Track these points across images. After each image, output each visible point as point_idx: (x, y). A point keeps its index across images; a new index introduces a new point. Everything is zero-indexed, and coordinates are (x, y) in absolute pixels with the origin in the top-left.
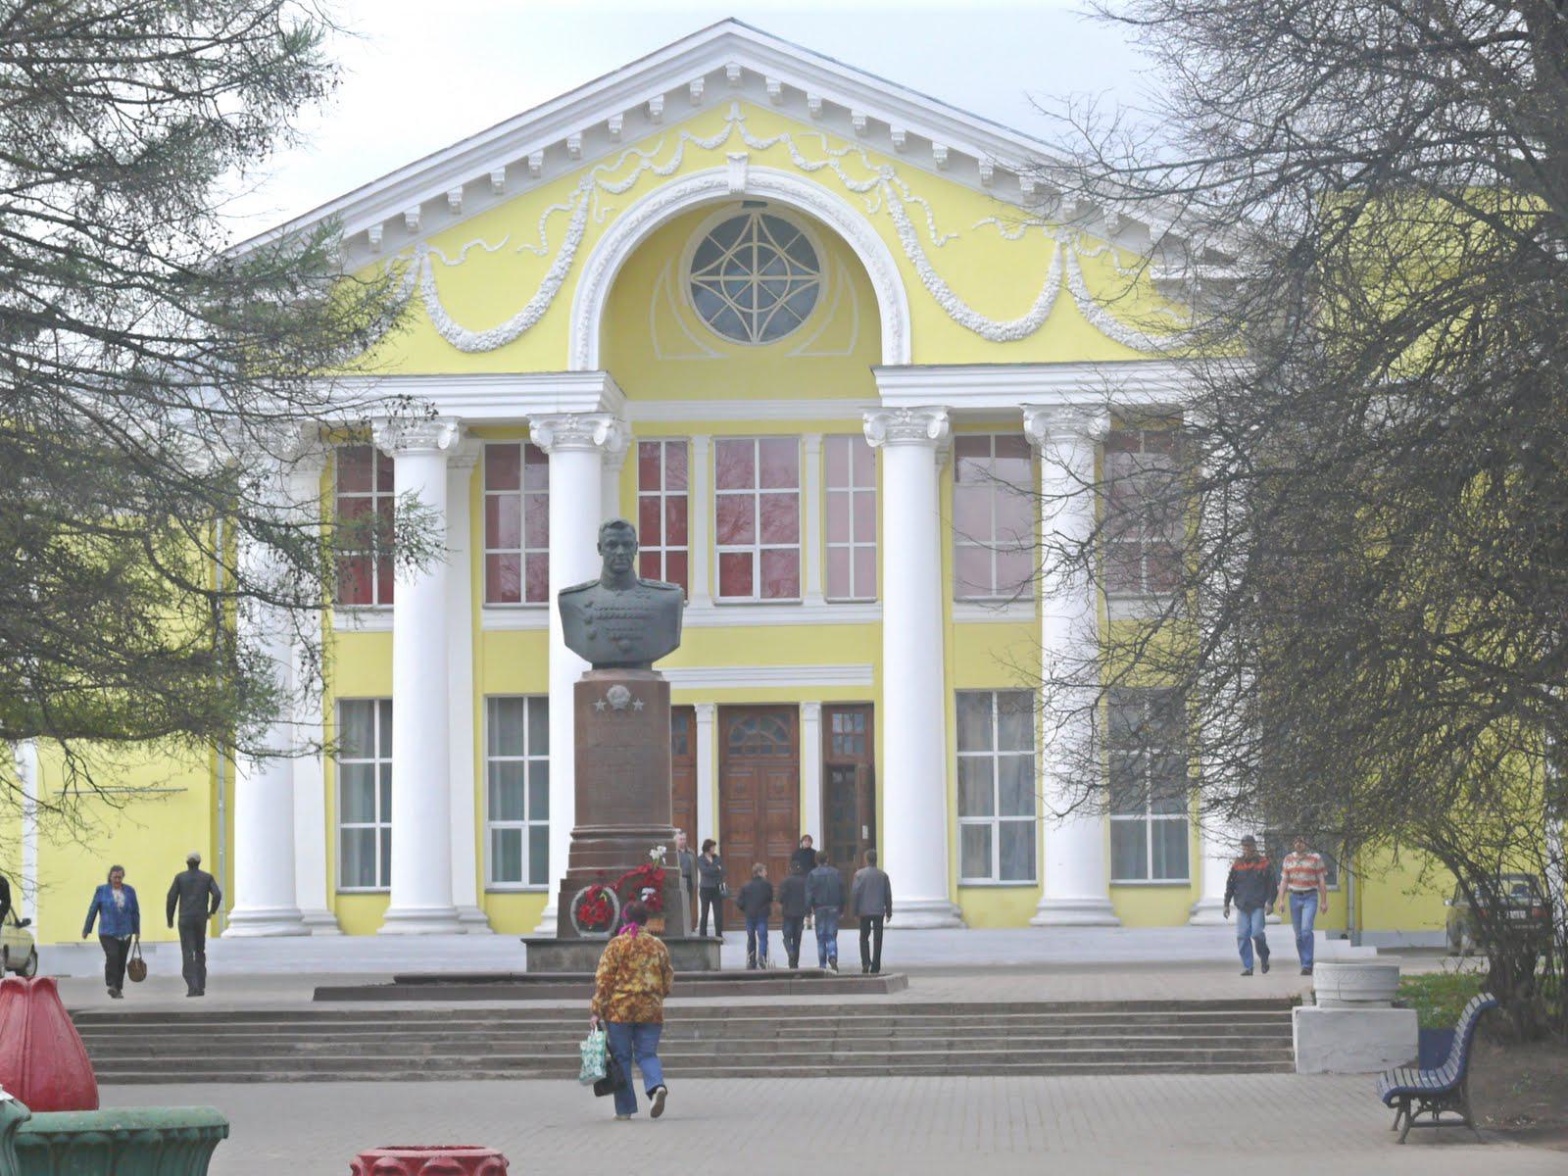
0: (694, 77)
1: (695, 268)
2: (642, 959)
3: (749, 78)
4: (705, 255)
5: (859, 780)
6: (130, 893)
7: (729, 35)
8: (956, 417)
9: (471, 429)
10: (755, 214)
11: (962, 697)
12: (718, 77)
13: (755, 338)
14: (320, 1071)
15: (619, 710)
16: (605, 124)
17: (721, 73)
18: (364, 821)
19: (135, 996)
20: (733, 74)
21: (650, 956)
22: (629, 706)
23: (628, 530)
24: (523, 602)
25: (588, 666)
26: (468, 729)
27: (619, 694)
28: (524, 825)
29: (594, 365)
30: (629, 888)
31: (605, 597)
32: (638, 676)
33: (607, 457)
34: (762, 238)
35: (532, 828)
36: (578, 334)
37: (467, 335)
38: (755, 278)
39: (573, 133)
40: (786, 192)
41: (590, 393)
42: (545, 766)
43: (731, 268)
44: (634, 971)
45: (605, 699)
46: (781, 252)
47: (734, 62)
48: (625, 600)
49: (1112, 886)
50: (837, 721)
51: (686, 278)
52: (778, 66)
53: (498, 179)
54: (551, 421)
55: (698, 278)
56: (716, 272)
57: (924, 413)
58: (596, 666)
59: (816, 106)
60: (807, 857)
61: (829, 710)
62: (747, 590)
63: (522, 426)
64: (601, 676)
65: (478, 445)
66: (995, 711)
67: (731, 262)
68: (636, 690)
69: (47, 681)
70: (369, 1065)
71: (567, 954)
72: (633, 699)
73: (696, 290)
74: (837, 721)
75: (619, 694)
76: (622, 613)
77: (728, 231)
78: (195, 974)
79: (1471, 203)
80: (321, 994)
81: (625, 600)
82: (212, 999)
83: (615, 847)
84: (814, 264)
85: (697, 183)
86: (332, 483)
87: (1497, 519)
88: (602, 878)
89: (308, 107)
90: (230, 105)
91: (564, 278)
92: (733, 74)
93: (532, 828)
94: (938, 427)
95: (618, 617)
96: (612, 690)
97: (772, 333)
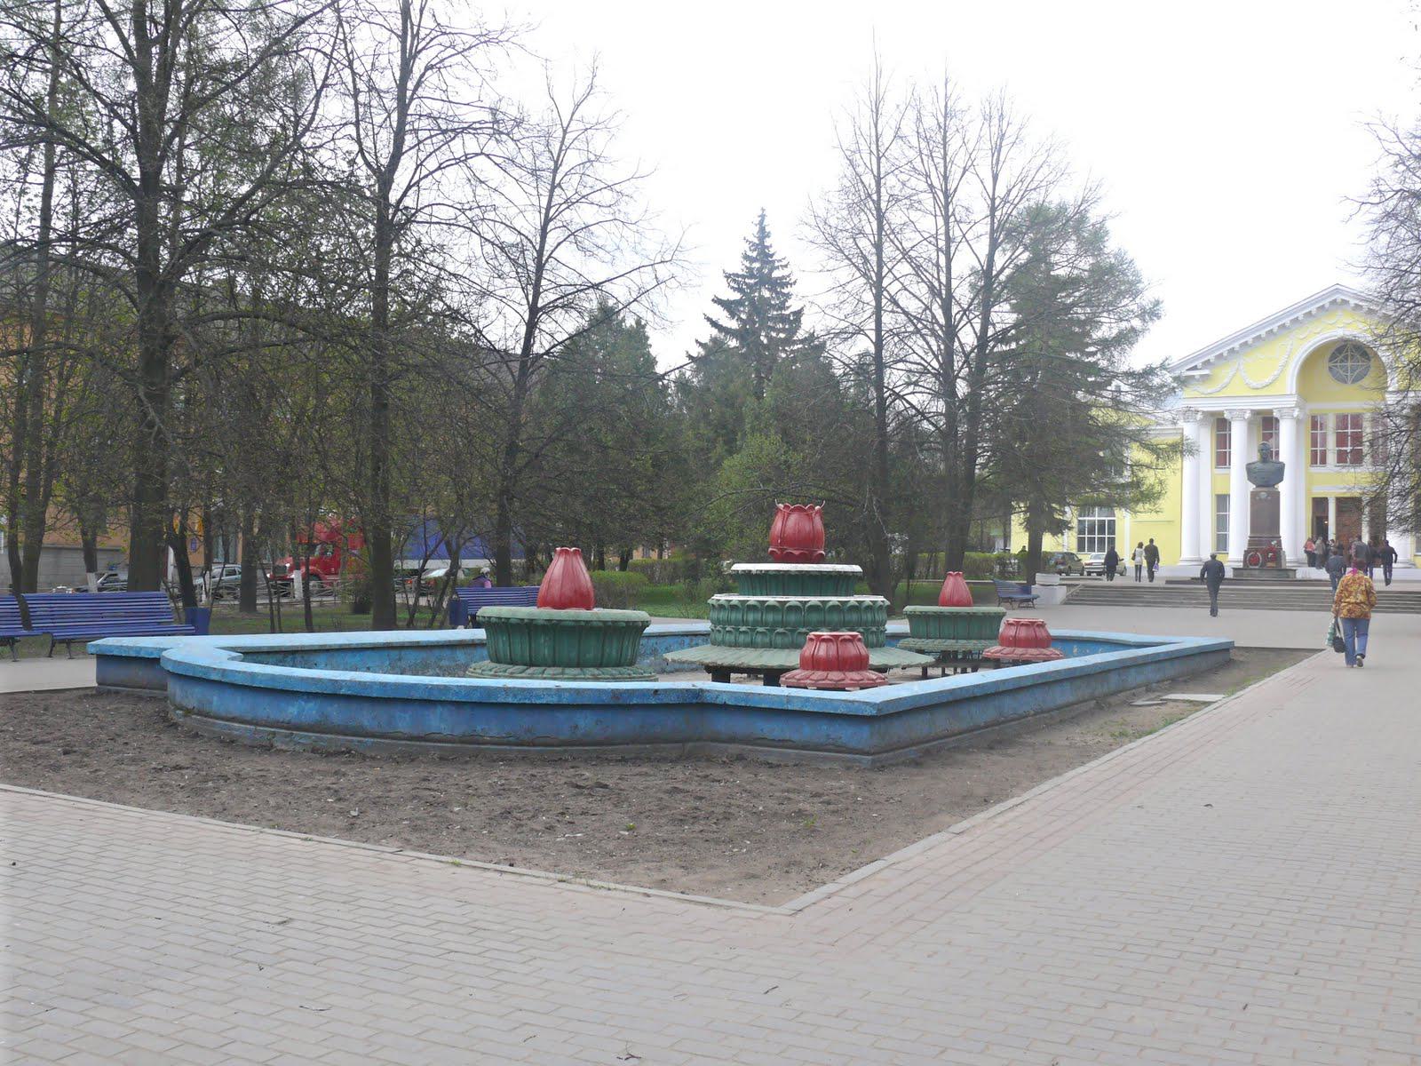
0: (1326, 302)
1: (1330, 361)
2: (1355, 587)
3: (1345, 302)
9: (1256, 413)
12: (1334, 302)
14: (1148, 604)
17: (1335, 300)
19: (1118, 581)
20: (1339, 301)
21: (1360, 585)
27: (1263, 495)
29: (1294, 392)
30: (1265, 553)
31: (1260, 465)
32: (1270, 489)
33: (1298, 421)
36: (1290, 383)
37: (1254, 384)
38: (1349, 364)
43: (1342, 361)
44: (1351, 592)
47: (1339, 297)
48: (1268, 467)
51: (1327, 364)
52: (1312, 305)
54: (1280, 410)
55: (1331, 364)
57: (1243, 411)
58: (1258, 486)
63: (1271, 411)
64: (1259, 489)
65: (1259, 418)
68: (1269, 494)
70: (1164, 603)
71: (1245, 572)
73: (1330, 368)
75: (1263, 495)
78: (1151, 576)
80: (1168, 582)
81: (1268, 467)
85: (1327, 335)
88: (1257, 550)
89: (1157, 322)
90: (1136, 323)
91: (1284, 366)
92: (1339, 301)
94: (1248, 415)
97: (1354, 381)
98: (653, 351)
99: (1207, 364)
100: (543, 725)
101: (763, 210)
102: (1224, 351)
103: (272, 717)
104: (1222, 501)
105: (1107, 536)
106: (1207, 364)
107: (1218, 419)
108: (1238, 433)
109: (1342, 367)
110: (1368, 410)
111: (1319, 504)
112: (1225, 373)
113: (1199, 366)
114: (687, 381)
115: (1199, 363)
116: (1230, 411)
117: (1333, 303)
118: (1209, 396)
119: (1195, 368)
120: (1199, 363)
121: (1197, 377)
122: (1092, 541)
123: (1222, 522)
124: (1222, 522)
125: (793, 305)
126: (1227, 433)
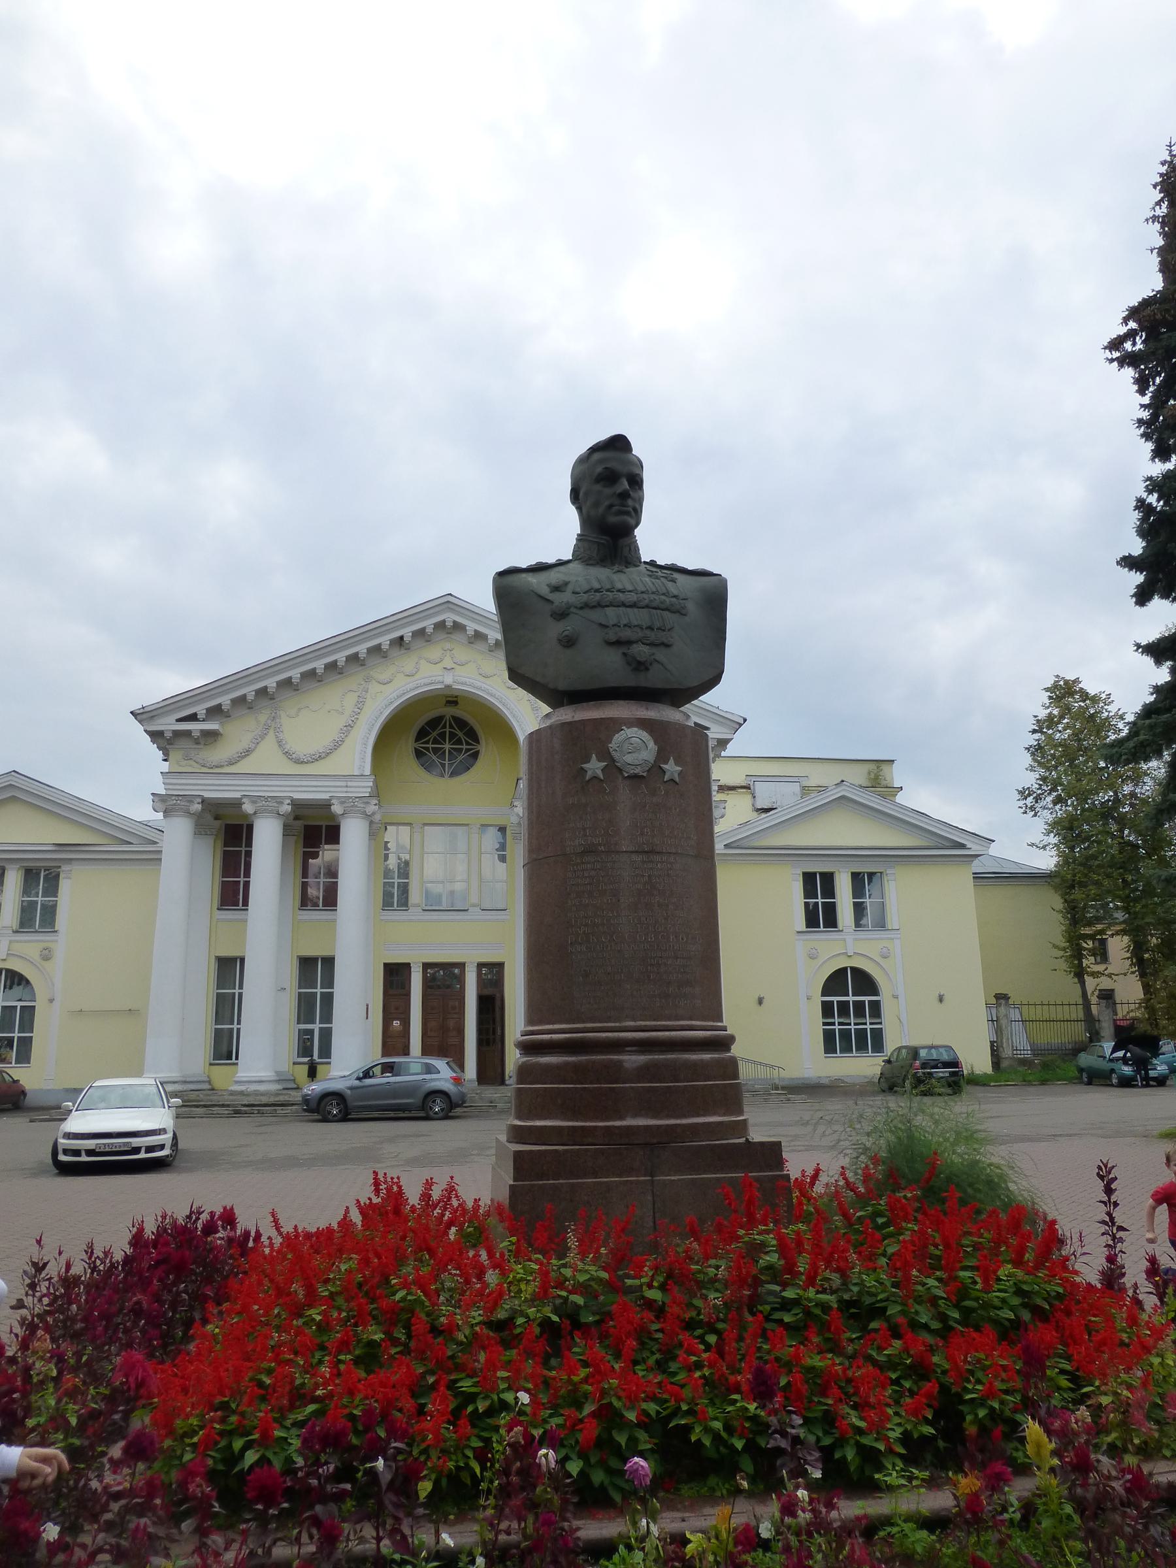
0: (429, 624)
1: (417, 739)
3: (458, 627)
4: (421, 735)
5: (498, 1003)
6: (400, 1187)
7: (448, 602)
8: (295, 804)
10: (625, 485)
11: (387, 967)
12: (440, 626)
13: (446, 776)
15: (635, 777)
16: (357, 654)
18: (222, 1029)
20: (449, 624)
22: (656, 769)
23: (1128, 1485)
24: (822, 928)
25: (546, 709)
26: (290, 973)
28: (316, 1027)
29: (368, 771)
34: (451, 726)
35: (321, 1029)
36: (356, 757)
38: (447, 746)
39: (295, 674)
40: (488, 693)
41: (364, 787)
42: (406, 885)
43: (435, 741)
45: (605, 755)
46: (460, 734)
47: (450, 617)
49: (211, 1064)
50: (484, 971)
52: (474, 620)
53: (320, 671)
56: (427, 742)
57: (279, 800)
59: (470, 632)
60: (1029, 1406)
61: (480, 966)
62: (32, 925)
65: (300, 824)
66: (621, 1057)
67: (435, 739)
69: (164, 1346)
72: (662, 756)
74: (484, 971)
76: (633, 597)
77: (435, 722)
79: (872, 1184)
82: (717, 797)
83: (674, 1071)
84: (478, 742)
86: (220, 844)
87: (761, 1312)
92: (449, 624)
93: (321, 1029)
94: (286, 808)
95: (624, 605)
96: (618, 738)
98: (573, 508)
99: (215, 712)
100: (392, 1114)
101: (1147, 220)
102: (385, 640)
103: (851, 1103)
104: (229, 969)
105: (319, 990)
106: (215, 712)
107: (227, 826)
108: (268, 841)
109: (435, 751)
110: (476, 1544)
111: (396, 974)
112: (238, 733)
113: (202, 713)
114: (842, 1446)
115: (200, 709)
116: (254, 800)
117: (440, 624)
118: (214, 770)
119: (193, 718)
120: (200, 709)
121: (196, 734)
122: (845, 1035)
123: (227, 1008)
124: (227, 1008)
125: (470, 1204)
126: (242, 879)
